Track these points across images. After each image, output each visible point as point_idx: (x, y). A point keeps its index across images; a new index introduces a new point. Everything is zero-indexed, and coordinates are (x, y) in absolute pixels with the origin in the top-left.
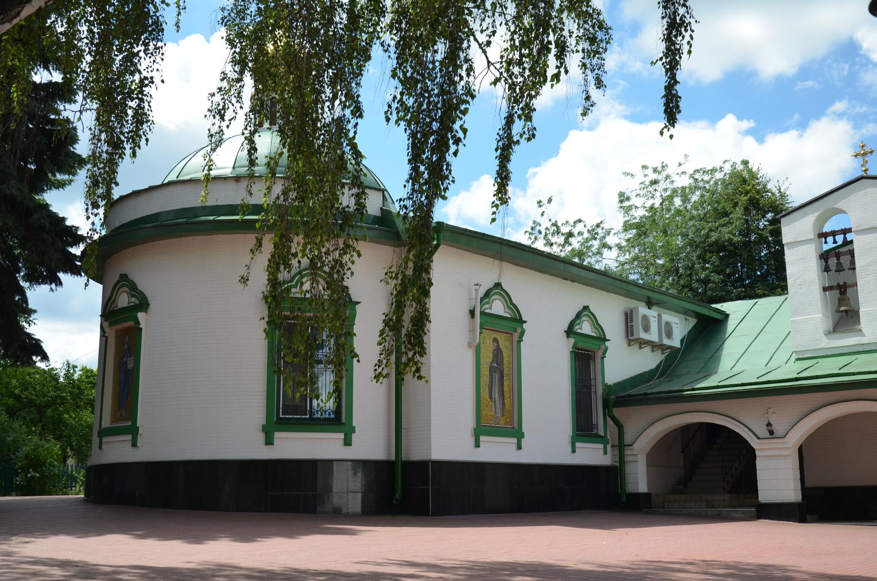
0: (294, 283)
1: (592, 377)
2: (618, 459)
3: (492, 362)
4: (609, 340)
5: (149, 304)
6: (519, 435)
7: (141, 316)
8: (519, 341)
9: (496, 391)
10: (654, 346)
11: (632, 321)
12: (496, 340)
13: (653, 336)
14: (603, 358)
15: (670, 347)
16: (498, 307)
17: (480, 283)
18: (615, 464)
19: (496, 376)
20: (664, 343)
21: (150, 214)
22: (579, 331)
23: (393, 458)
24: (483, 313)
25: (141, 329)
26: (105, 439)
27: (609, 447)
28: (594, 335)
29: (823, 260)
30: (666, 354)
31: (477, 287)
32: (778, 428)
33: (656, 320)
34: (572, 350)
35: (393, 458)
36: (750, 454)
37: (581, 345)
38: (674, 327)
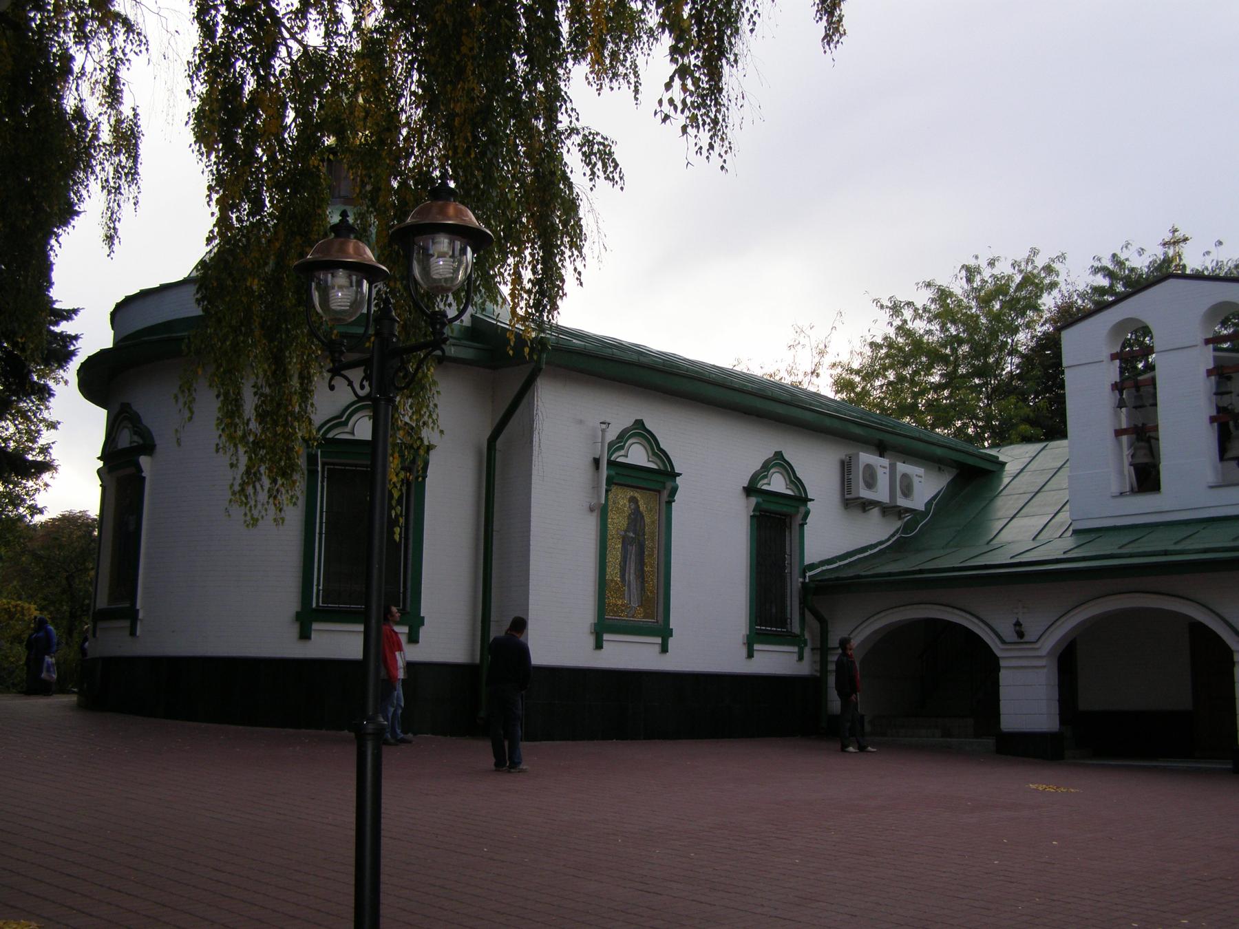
0: (343, 419)
1: (788, 551)
2: (818, 668)
3: (626, 531)
4: (813, 500)
5: (155, 446)
6: (664, 633)
7: (144, 461)
8: (669, 503)
9: (632, 571)
10: (889, 510)
11: (849, 472)
12: (633, 500)
13: (881, 493)
14: (802, 526)
15: (908, 510)
16: (637, 455)
17: (608, 421)
18: (815, 673)
19: (633, 549)
20: (898, 504)
21: (160, 322)
22: (765, 487)
23: (477, 661)
24: (612, 464)
25: (144, 478)
26: (101, 625)
27: (807, 652)
28: (790, 492)
29: (1117, 392)
30: (906, 519)
31: (604, 426)
32: (1032, 631)
33: (887, 471)
34: (752, 514)
35: (477, 661)
36: (991, 665)
37: (765, 506)
38: (916, 481)
